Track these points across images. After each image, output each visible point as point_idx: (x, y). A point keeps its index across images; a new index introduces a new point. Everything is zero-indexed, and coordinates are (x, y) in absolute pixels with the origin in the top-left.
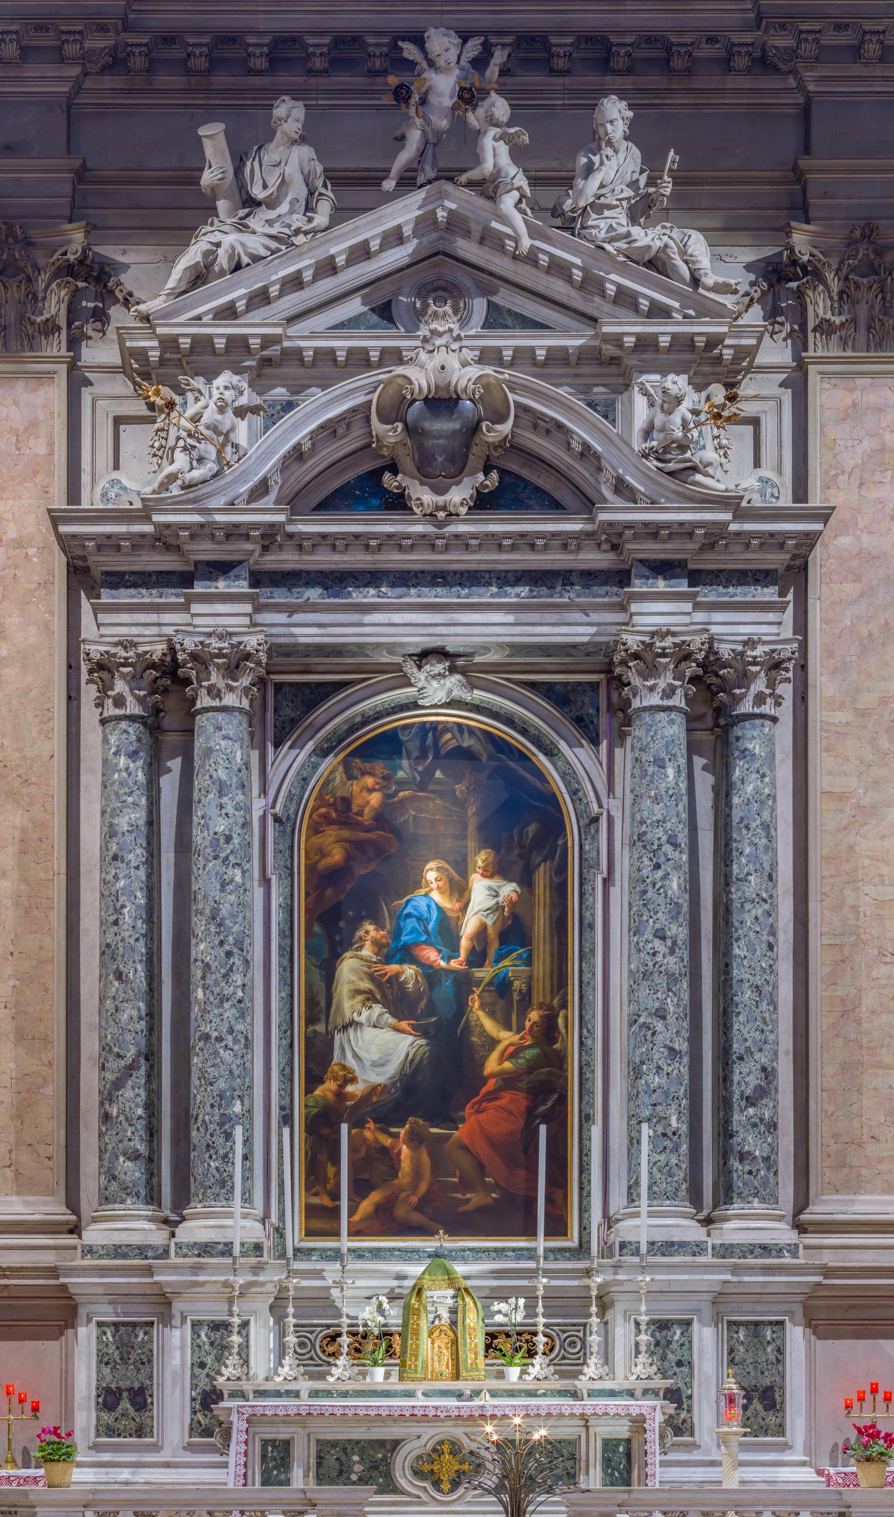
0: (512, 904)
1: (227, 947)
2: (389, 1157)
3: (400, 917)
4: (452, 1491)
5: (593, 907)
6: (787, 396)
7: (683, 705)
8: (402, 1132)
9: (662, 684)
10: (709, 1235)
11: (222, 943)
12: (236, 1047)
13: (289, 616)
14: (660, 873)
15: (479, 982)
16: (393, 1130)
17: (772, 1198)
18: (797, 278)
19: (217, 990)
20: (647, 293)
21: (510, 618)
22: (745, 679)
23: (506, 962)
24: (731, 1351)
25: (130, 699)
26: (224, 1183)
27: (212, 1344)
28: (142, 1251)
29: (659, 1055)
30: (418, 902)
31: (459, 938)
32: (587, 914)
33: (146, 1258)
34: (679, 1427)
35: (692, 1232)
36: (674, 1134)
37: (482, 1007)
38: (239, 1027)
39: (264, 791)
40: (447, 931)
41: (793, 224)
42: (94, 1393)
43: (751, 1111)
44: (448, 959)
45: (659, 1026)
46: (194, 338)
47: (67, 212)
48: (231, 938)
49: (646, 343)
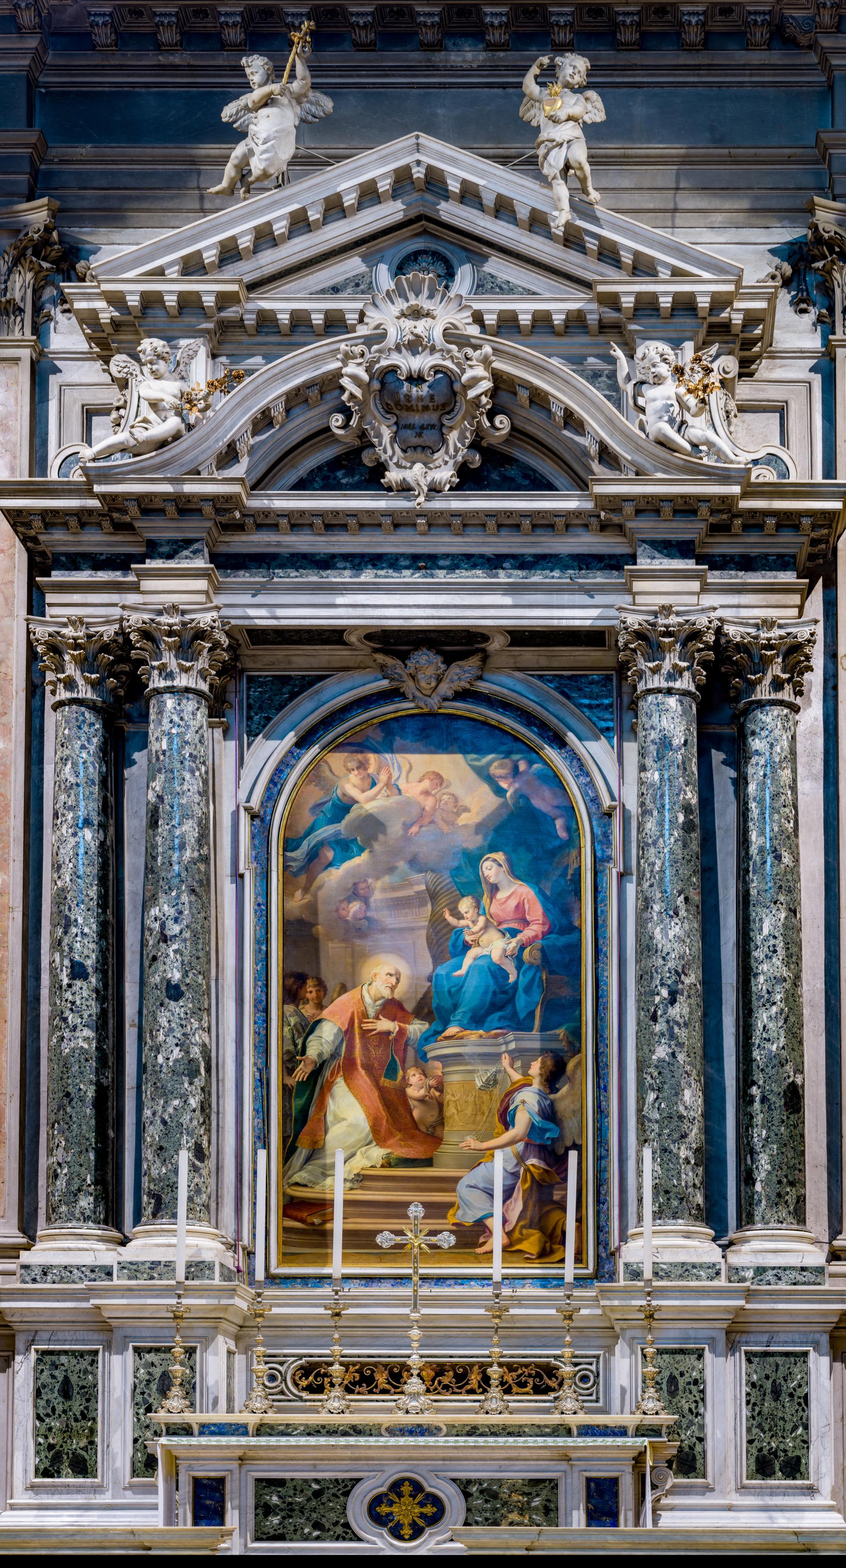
6: (817, 380)
7: (692, 689)
9: (667, 666)
13: (254, 596)
17: (799, 1215)
18: (824, 257)
21: (507, 600)
22: (765, 663)
25: (81, 682)
35: (710, 1253)
41: (817, 199)
47: (24, 189)
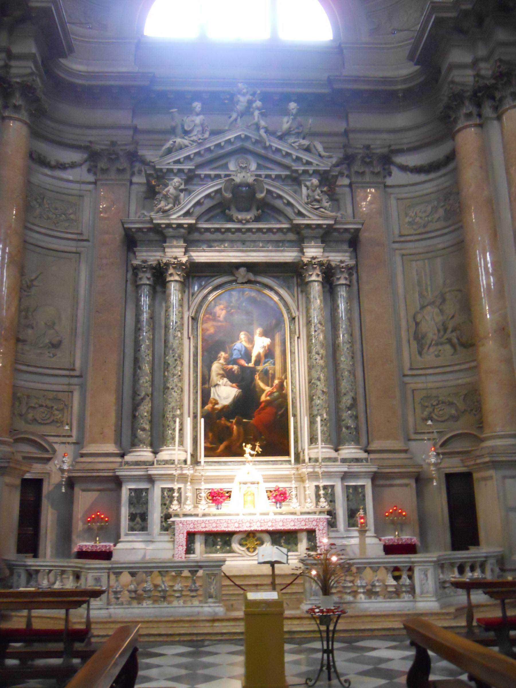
0: (269, 346)
1: (175, 358)
2: (229, 430)
3: (232, 350)
4: (254, 551)
5: (294, 347)
8: (234, 421)
10: (338, 454)
11: (174, 356)
12: (178, 391)
14: (316, 333)
15: (258, 371)
16: (231, 420)
19: (172, 372)
20: (305, 157)
23: (267, 364)
24: (348, 497)
26: (173, 439)
27: (168, 497)
28: (144, 463)
29: (319, 393)
30: (238, 345)
31: (251, 357)
32: (293, 349)
33: (147, 465)
34: (332, 524)
36: (325, 420)
37: (259, 379)
38: (179, 385)
39: (189, 309)
40: (247, 355)
42: (128, 515)
43: (349, 412)
44: (248, 363)
45: (319, 383)
46: (168, 169)
48: (177, 355)
49: (305, 172)
